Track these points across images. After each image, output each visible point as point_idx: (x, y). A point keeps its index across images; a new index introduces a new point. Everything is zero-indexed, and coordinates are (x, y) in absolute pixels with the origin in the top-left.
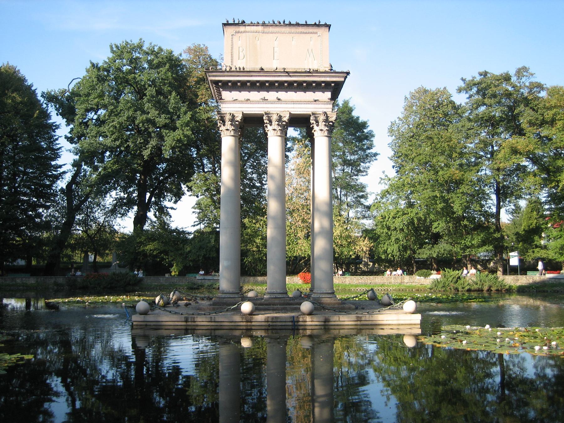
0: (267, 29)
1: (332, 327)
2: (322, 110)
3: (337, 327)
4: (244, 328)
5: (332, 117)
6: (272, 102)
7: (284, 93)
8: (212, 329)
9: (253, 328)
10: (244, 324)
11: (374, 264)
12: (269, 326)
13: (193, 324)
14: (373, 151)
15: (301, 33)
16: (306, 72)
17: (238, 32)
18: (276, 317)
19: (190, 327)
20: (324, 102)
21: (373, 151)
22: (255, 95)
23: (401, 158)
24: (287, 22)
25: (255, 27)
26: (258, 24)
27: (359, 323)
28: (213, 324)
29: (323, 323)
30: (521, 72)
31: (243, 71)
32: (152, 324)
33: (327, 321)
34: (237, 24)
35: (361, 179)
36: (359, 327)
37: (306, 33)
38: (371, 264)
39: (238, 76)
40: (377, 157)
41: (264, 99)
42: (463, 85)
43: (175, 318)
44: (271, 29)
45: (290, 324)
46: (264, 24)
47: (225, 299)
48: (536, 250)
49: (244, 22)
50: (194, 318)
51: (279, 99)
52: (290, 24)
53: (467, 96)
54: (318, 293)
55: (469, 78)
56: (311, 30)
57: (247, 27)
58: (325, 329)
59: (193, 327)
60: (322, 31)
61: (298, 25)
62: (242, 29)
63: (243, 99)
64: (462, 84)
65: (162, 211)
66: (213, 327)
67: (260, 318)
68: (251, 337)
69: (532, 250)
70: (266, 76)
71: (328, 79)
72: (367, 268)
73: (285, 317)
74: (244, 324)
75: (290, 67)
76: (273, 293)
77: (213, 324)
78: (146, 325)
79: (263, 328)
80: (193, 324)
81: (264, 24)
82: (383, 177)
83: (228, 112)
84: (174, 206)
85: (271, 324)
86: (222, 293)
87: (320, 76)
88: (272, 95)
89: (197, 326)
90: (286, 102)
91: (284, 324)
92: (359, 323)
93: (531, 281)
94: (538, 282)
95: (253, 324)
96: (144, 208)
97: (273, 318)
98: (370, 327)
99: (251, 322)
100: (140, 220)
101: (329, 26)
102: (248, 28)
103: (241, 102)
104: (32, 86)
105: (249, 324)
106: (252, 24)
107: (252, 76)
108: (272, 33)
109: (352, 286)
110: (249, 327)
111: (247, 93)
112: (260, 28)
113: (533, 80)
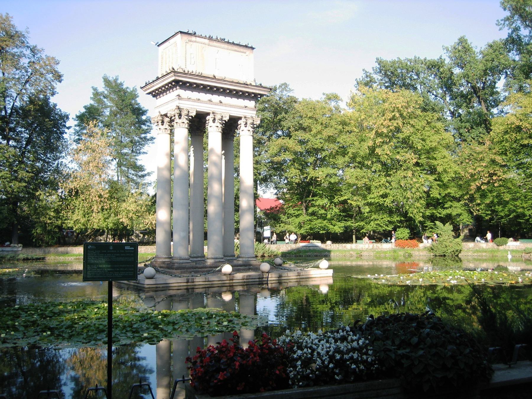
2: (251, 115)
3: (304, 280)
4: (228, 285)
5: (192, 113)
6: (216, 104)
7: (204, 94)
8: (205, 288)
9: (234, 284)
10: (228, 282)
11: (144, 236)
12: (244, 282)
13: (192, 284)
14: (148, 136)
15: (235, 51)
16: (242, 84)
18: (249, 276)
19: (190, 287)
20: (251, 109)
21: (148, 136)
22: (203, 96)
24: (226, 40)
25: (203, 39)
26: (205, 38)
27: (298, 277)
28: (207, 283)
29: (277, 279)
30: (285, 86)
31: (200, 76)
32: (161, 286)
33: (280, 276)
34: (190, 34)
35: (141, 160)
36: (298, 280)
37: (238, 51)
38: (142, 235)
39: (197, 79)
40: (155, 141)
41: (210, 101)
43: (179, 280)
44: (215, 44)
45: (258, 280)
46: (210, 38)
47: (183, 264)
48: (282, 225)
50: (193, 279)
52: (228, 42)
54: (246, 258)
56: (242, 49)
57: (197, 38)
58: (279, 282)
59: (192, 287)
60: (248, 51)
62: (193, 38)
63: (195, 98)
66: (206, 286)
67: (239, 276)
68: (233, 293)
69: (279, 225)
70: (216, 82)
71: (257, 92)
72: (138, 239)
73: (255, 275)
74: (228, 282)
76: (217, 258)
77: (207, 283)
78: (157, 287)
79: (241, 284)
80: (192, 284)
81: (210, 38)
83: (185, 108)
85: (245, 280)
86: (180, 259)
87: (252, 89)
88: (216, 98)
89: (195, 285)
90: (226, 105)
91: (254, 280)
92: (298, 277)
93: (289, 249)
94: (295, 250)
95: (234, 281)
97: (247, 276)
99: (233, 280)
101: (252, 48)
102: (198, 39)
103: (194, 101)
104: (118, 79)
105: (231, 281)
106: (200, 37)
107: (206, 81)
109: (149, 254)
110: (231, 284)
111: (211, 95)
112: (206, 41)
113: (291, 94)
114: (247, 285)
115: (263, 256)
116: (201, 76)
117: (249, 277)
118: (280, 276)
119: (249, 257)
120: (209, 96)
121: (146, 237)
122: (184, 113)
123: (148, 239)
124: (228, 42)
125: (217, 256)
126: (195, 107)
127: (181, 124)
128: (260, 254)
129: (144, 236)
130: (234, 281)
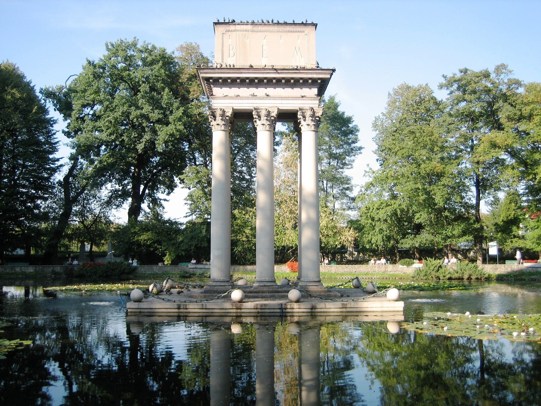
0: (256, 28)
1: (319, 314)
2: (308, 105)
4: (234, 314)
5: (318, 113)
6: (261, 98)
8: (203, 316)
9: (243, 314)
10: (234, 311)
11: (359, 253)
12: (258, 312)
13: (185, 311)
14: (358, 145)
16: (293, 69)
17: (229, 31)
18: (265, 305)
19: (182, 314)
20: (311, 98)
21: (358, 145)
22: (244, 91)
23: (385, 152)
24: (275, 21)
25: (245, 26)
26: (247, 23)
27: (344, 310)
28: (204, 311)
29: (310, 310)
30: (500, 69)
31: (233, 69)
32: (146, 311)
35: (347, 172)
36: (344, 314)
37: (294, 32)
38: (356, 253)
39: (228, 73)
40: (362, 151)
42: (444, 82)
43: (168, 305)
44: (260, 28)
45: (279, 311)
46: (253, 23)
47: (216, 287)
48: (514, 240)
49: (234, 21)
50: (186, 305)
51: (268, 95)
53: (448, 92)
54: (305, 281)
55: (450, 75)
56: (298, 28)
57: (237, 26)
58: (311, 315)
59: (185, 314)
61: (286, 24)
62: (232, 27)
63: (233, 95)
64: (443, 81)
65: (155, 202)
67: (250, 305)
69: (510, 240)
70: (255, 73)
71: (315, 76)
73: (274, 305)
75: (279, 65)
78: (140, 312)
80: (185, 311)
81: (253, 23)
82: (368, 170)
83: (219, 108)
84: (167, 198)
85: (260, 311)
86: (213, 281)
88: (261, 91)
89: (189, 312)
90: (275, 98)
91: (272, 311)
92: (344, 310)
93: (509, 270)
94: (516, 271)
95: (243, 311)
96: (138, 199)
97: (262, 305)
98: (355, 314)
99: (241, 309)
100: (134, 211)
101: (316, 25)
102: (238, 27)
103: (231, 98)
104: (31, 83)
105: (239, 311)
106: (241, 23)
107: (241, 73)
108: (261, 31)
109: (338, 274)
110: (239, 314)
112: (249, 27)
113: (511, 77)
114: (261, 316)
115: (469, 279)
116: (234, 69)
117: (263, 307)
118: (313, 308)
119: (308, 282)
120: (253, 90)
121: (361, 255)
122: (218, 113)
123: (364, 257)
124: (278, 23)
125: (263, 279)
126: (276, 105)
127: (216, 126)
128: (466, 276)
129: (359, 253)
130: (243, 311)
